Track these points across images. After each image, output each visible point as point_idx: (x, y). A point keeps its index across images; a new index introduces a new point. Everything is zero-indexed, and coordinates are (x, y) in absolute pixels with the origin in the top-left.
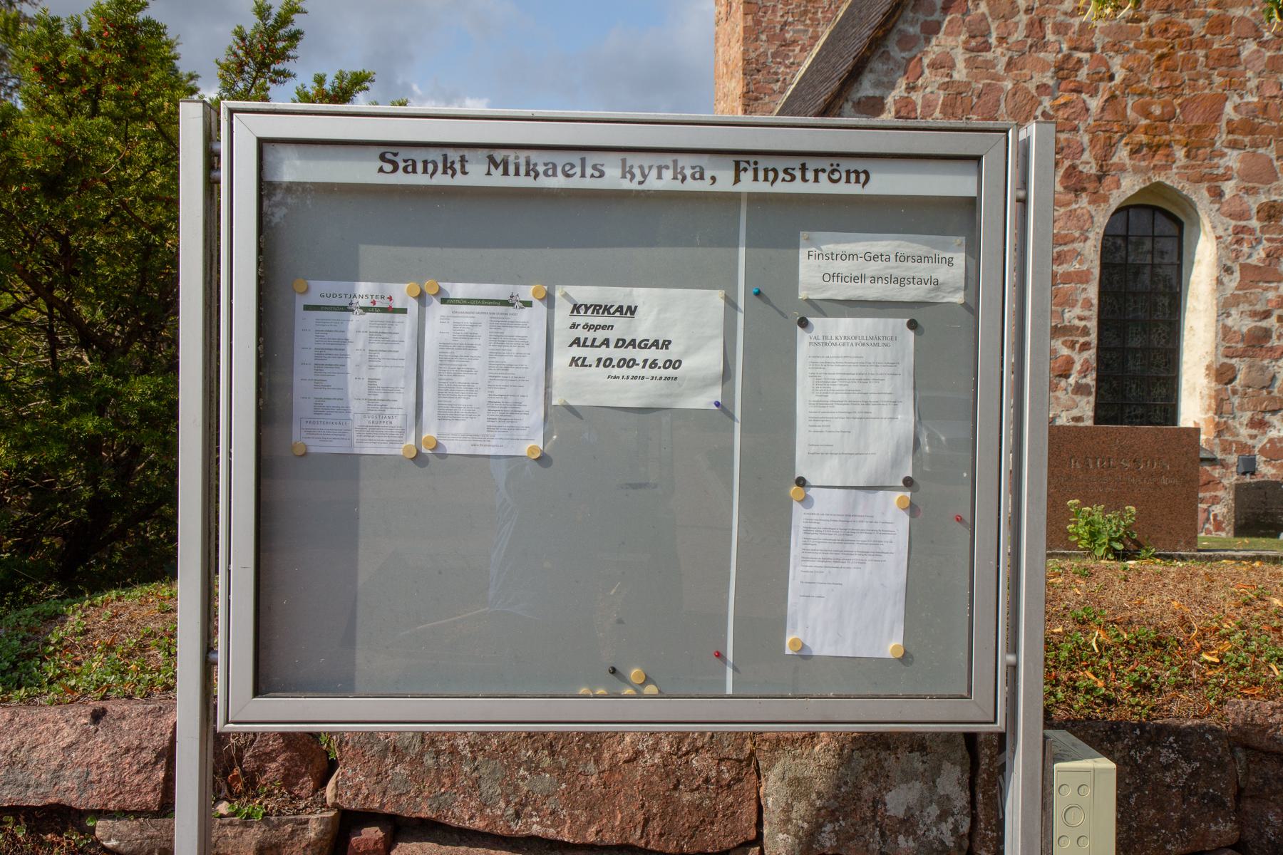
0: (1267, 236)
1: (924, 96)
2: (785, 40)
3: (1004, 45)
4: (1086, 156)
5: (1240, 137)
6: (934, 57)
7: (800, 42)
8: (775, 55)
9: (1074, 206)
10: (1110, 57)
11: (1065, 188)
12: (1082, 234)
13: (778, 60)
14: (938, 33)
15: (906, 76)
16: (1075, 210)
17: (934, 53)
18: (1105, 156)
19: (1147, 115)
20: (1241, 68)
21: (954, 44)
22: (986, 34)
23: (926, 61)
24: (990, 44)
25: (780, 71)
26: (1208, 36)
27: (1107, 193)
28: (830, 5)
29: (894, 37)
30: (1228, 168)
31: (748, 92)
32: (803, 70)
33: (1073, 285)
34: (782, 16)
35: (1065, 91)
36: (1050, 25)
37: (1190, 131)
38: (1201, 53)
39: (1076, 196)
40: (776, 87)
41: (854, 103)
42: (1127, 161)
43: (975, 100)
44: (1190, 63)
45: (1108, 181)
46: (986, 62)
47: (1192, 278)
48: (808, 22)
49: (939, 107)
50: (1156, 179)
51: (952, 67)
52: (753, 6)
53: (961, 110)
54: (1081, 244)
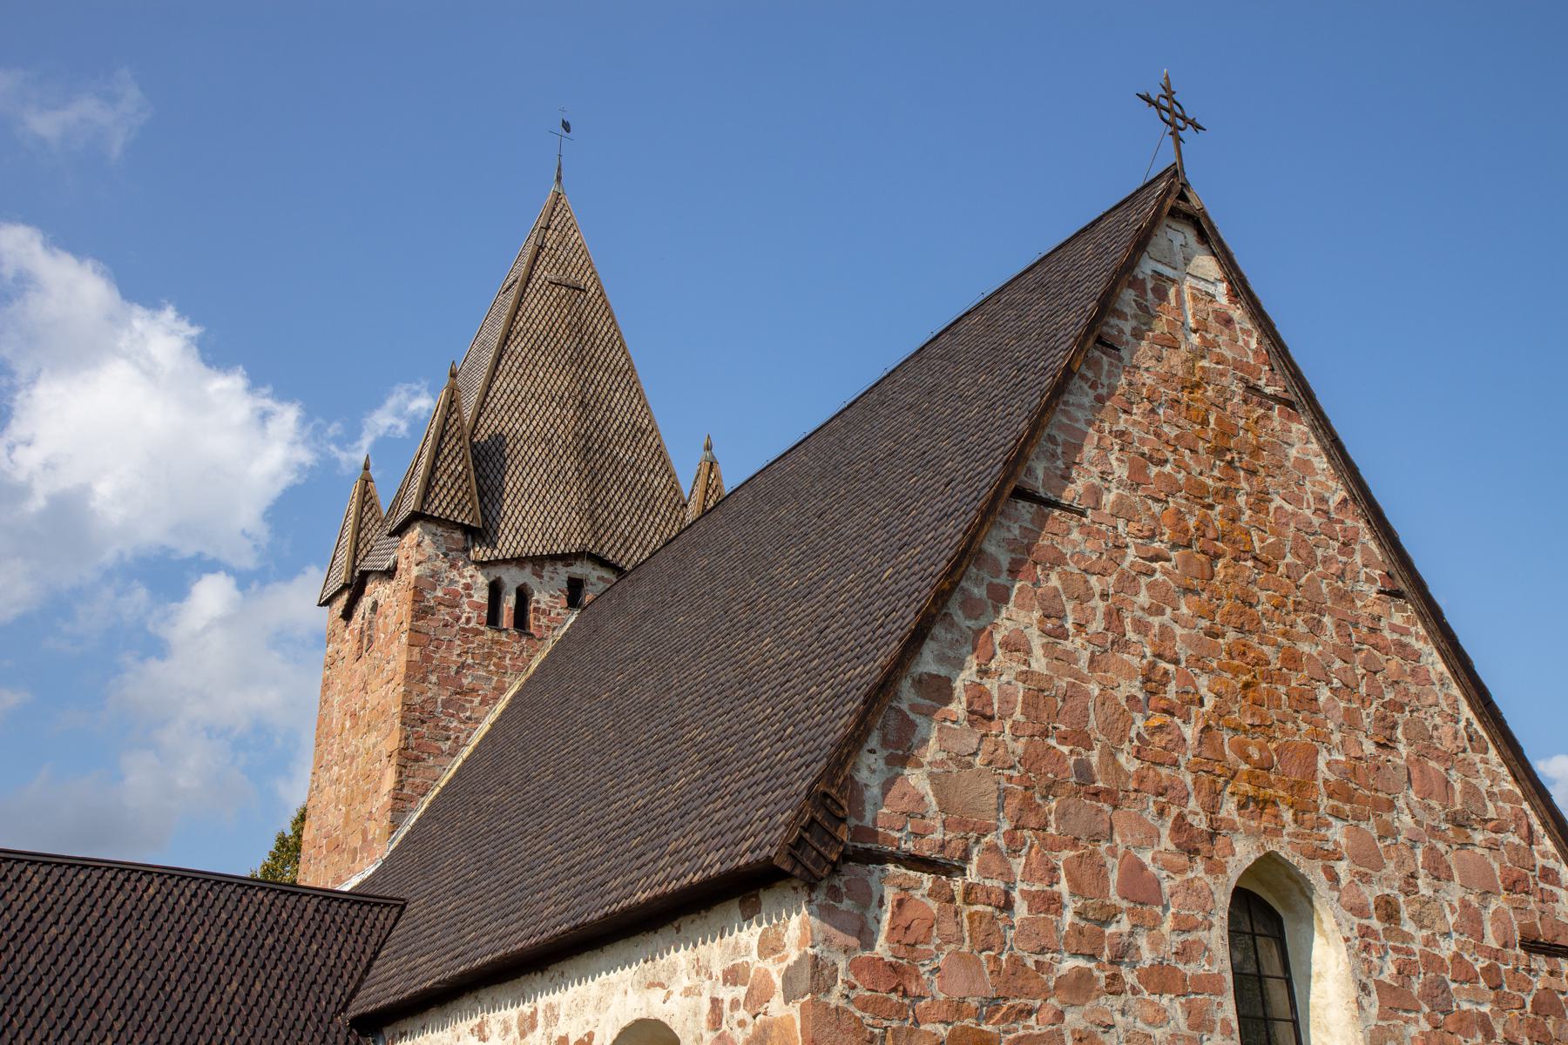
0: (1392, 943)
1: (999, 686)
2: (461, 686)
3: (1084, 635)
4: (1193, 804)
5: (1340, 804)
6: (1006, 633)
7: (480, 692)
8: (446, 704)
9: (1190, 875)
10: (1195, 674)
11: (1178, 846)
12: (1205, 918)
13: (451, 711)
14: (1007, 603)
15: (976, 654)
16: (1192, 880)
17: (1006, 629)
18: (1213, 806)
19: (1247, 758)
20: (1322, 716)
21: (1027, 620)
22: (1061, 616)
23: (998, 638)
24: (1067, 630)
25: (452, 726)
26: (1284, 670)
27: (1223, 860)
28: (521, 652)
29: (957, 597)
31: (407, 749)
32: (485, 727)
33: (1206, 996)
34: (459, 655)
35: (1156, 711)
36: (1129, 620)
37: (1292, 786)
39: (1190, 860)
40: (446, 746)
41: (913, 680)
43: (1060, 704)
45: (1220, 842)
46: (1066, 652)
47: (1313, 1000)
48: (492, 668)
49: (1019, 705)
51: (1029, 652)
52: (422, 636)
53: (1045, 715)
54: (1206, 932)
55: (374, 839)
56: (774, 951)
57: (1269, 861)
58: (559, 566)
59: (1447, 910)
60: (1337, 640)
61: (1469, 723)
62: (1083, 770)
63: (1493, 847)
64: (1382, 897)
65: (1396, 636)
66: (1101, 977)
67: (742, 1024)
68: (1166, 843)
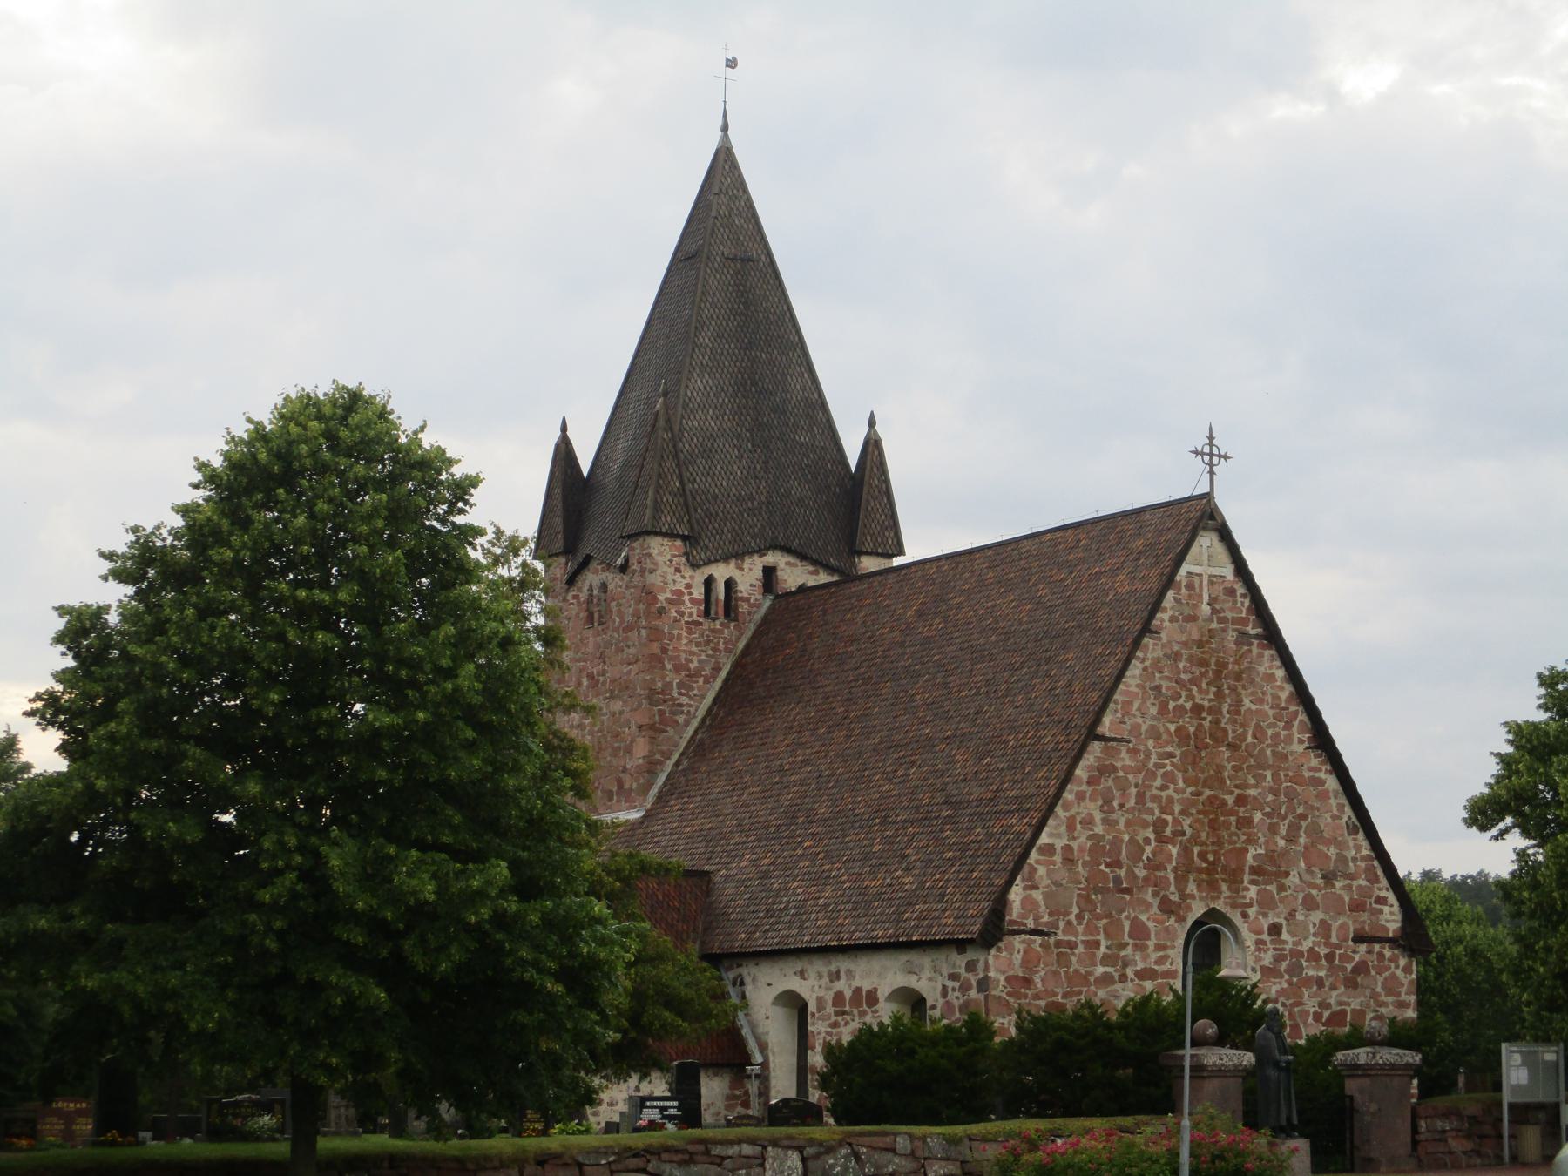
30: (1251, 899)
38: (1232, 818)
42: (1195, 892)
44: (1227, 825)
48: (710, 652)
50: (1212, 906)
55: (631, 789)
56: (972, 971)
57: (1212, 914)
58: (756, 557)
59: (1311, 926)
60: (1272, 784)
61: (1349, 818)
62: (1117, 880)
63: (1348, 888)
64: (1273, 924)
65: (1311, 774)
66: (1116, 976)
67: (957, 998)
68: (1155, 909)
